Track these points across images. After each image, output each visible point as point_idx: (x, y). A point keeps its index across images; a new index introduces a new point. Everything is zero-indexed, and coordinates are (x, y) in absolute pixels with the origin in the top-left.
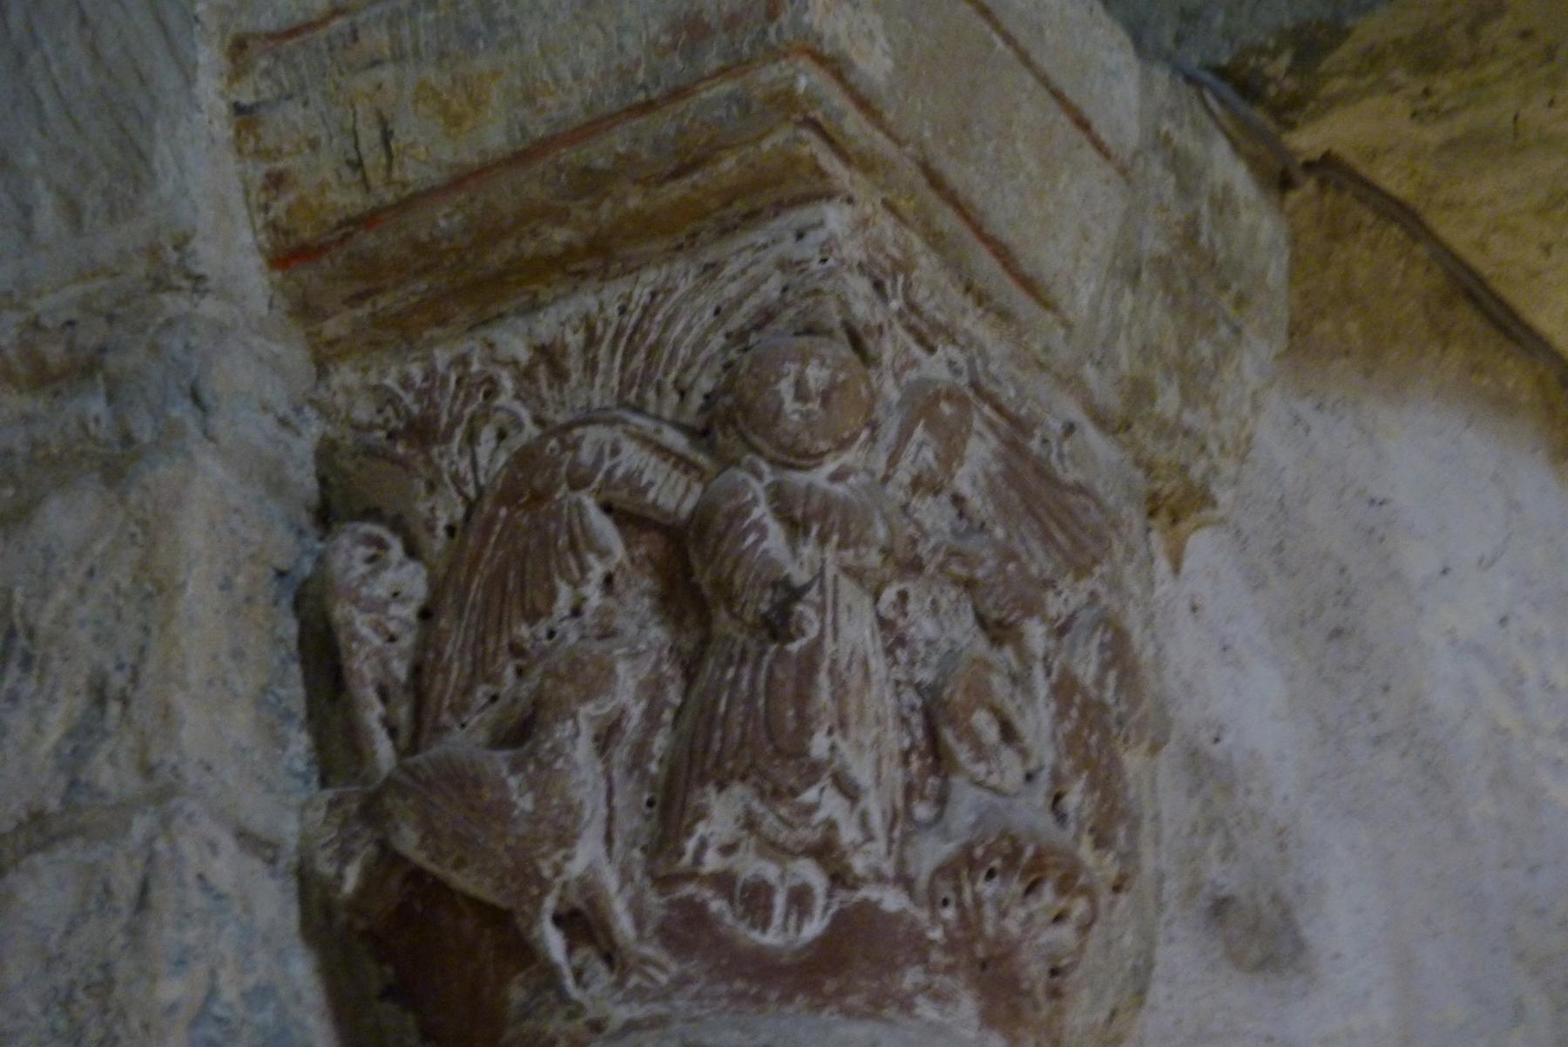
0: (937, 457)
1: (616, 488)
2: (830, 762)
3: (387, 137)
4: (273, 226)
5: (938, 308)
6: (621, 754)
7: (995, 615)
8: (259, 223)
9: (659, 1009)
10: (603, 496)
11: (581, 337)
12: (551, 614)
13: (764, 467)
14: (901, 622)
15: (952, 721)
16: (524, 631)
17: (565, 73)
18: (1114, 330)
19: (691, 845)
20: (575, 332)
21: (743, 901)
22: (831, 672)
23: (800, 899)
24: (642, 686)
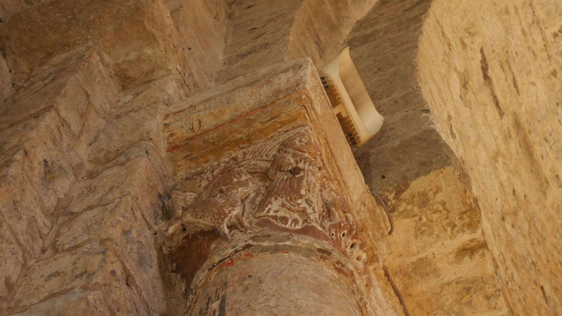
8: (166, 142)
19: (267, 209)
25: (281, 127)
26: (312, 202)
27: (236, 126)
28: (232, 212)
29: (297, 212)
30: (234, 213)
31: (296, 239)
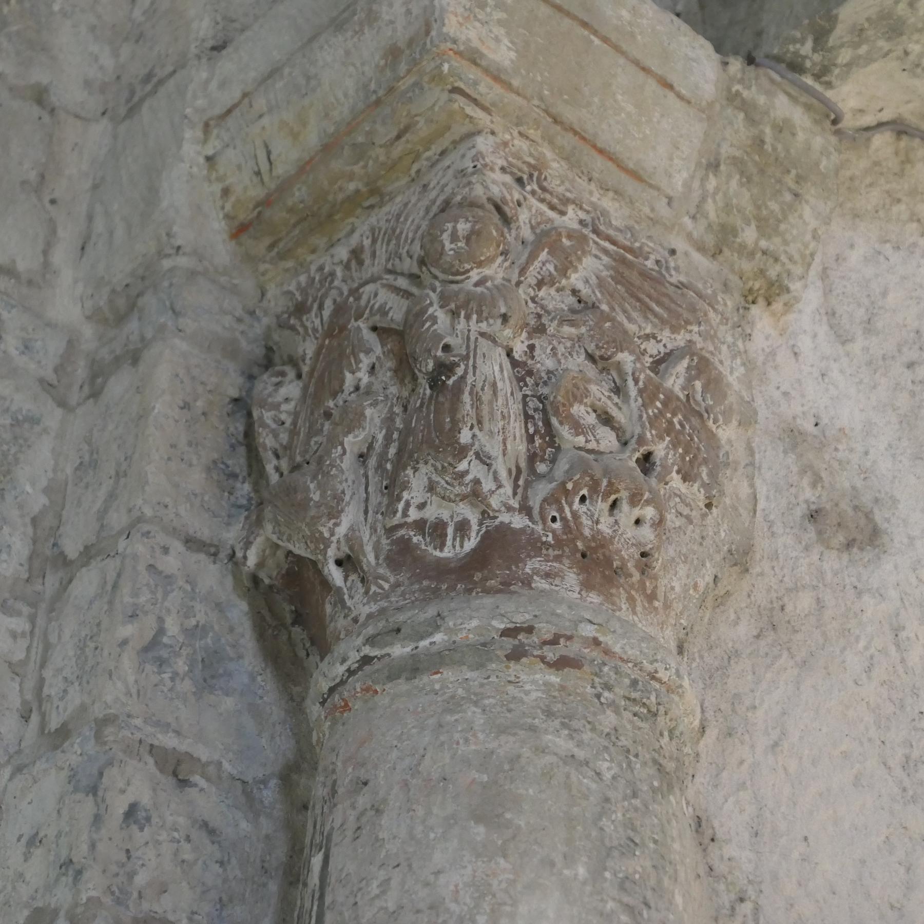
0: (556, 267)
1: (375, 315)
2: (472, 445)
3: (269, 153)
4: (227, 217)
5: (568, 190)
6: (372, 462)
7: (598, 353)
8: (221, 216)
9: (383, 604)
10: (371, 324)
11: (370, 240)
12: (343, 391)
13: (437, 284)
14: (530, 362)
15: (557, 413)
16: (331, 404)
17: (340, 95)
18: (703, 199)
20: (367, 238)
21: (430, 535)
22: (471, 393)
23: (462, 528)
24: (384, 421)
25: (428, 149)
26: (489, 458)
27: (336, 165)
28: (337, 529)
29: (461, 500)
30: (342, 530)
31: (451, 624)
